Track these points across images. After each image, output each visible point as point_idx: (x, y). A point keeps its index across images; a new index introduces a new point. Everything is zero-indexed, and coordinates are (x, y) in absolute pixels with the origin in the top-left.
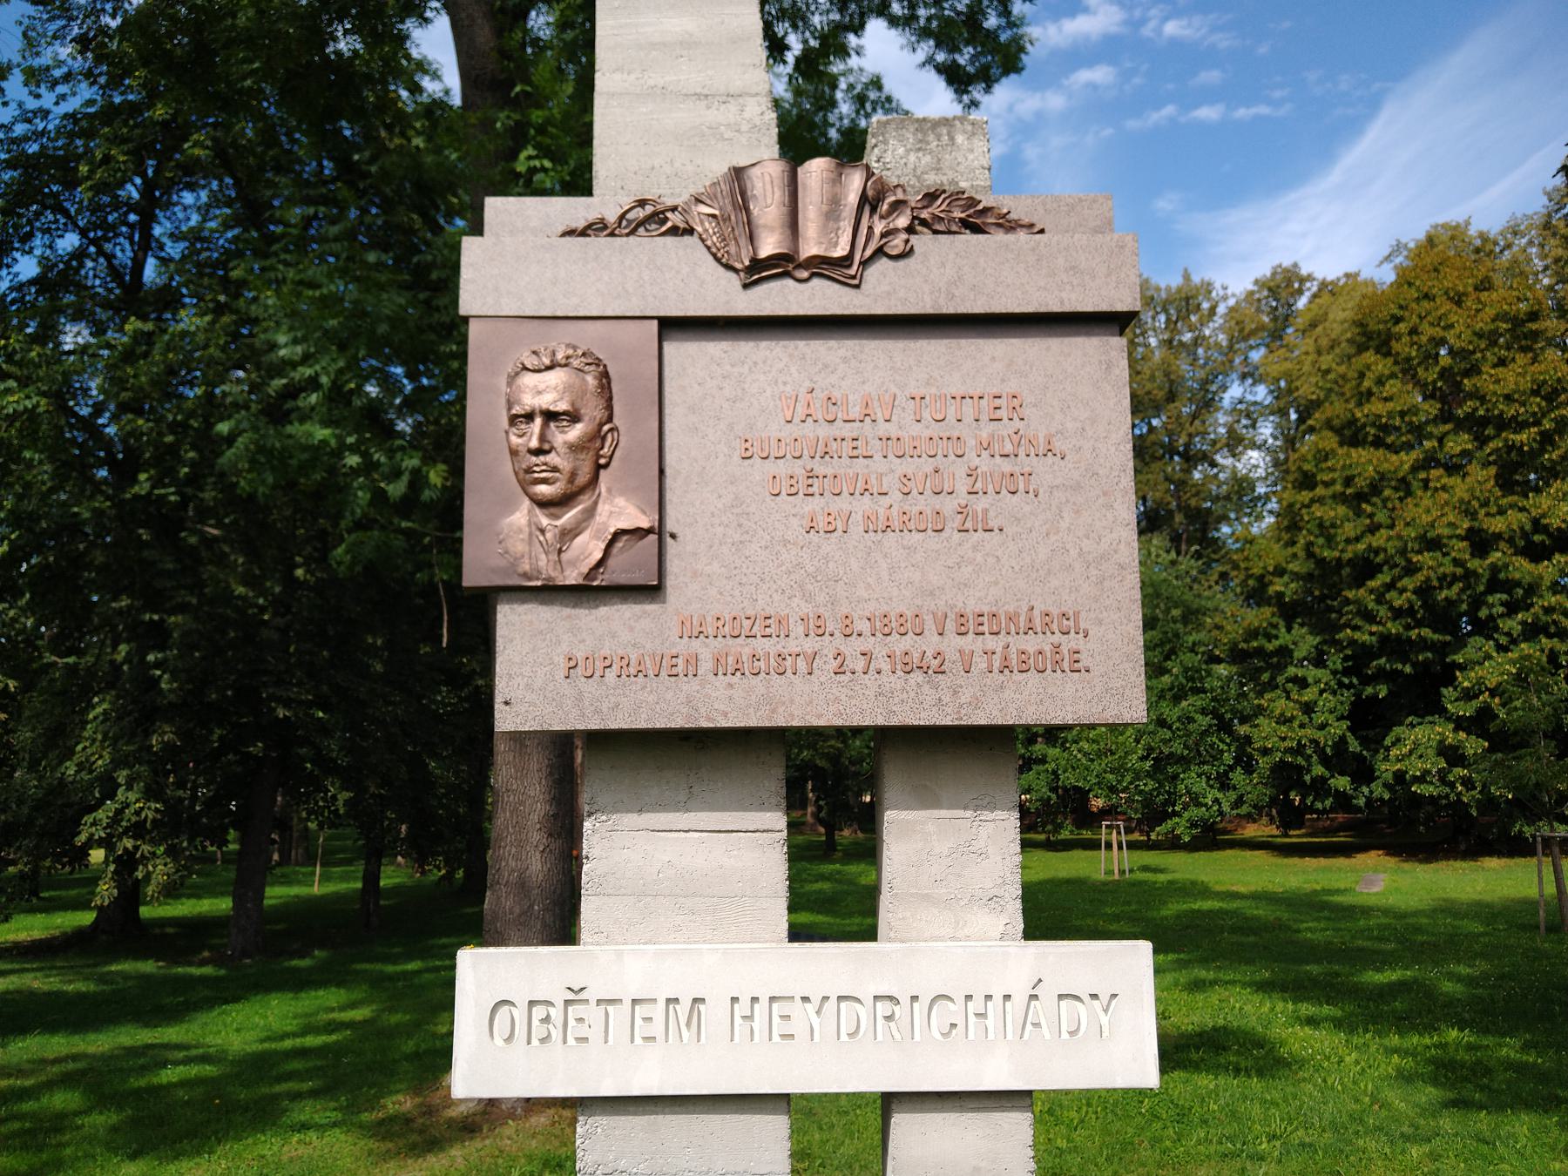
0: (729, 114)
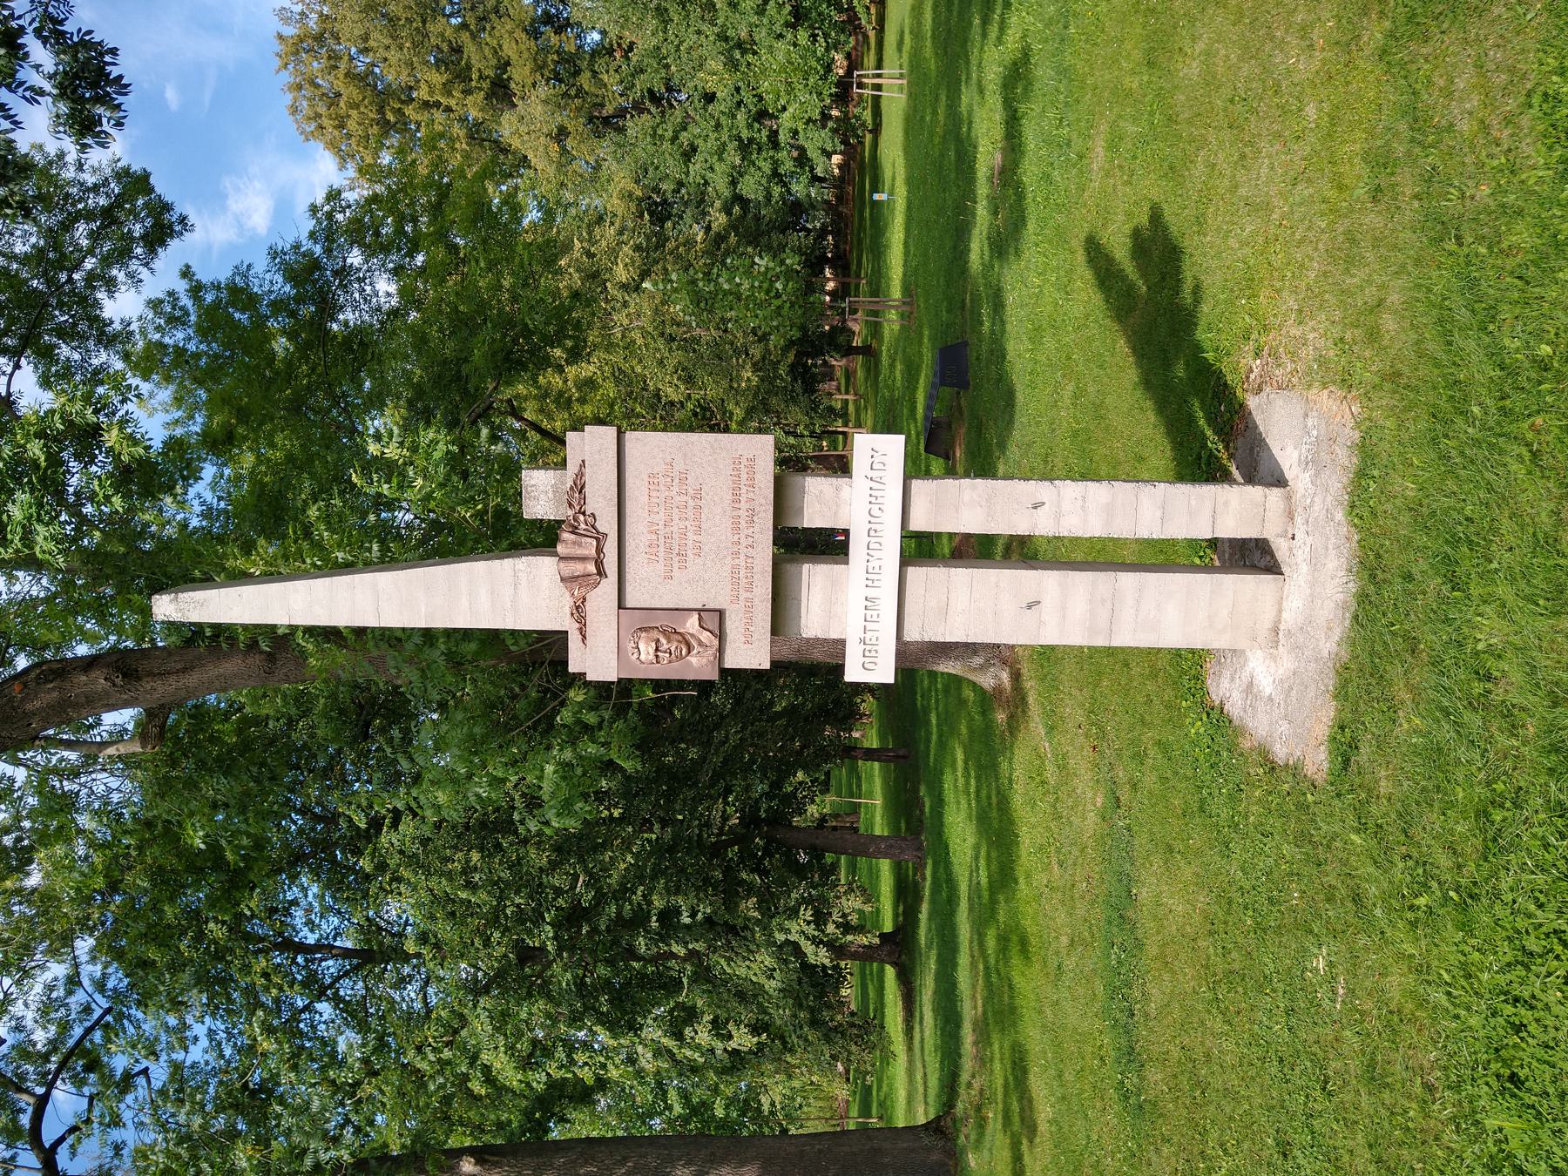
0: (523, 577)
